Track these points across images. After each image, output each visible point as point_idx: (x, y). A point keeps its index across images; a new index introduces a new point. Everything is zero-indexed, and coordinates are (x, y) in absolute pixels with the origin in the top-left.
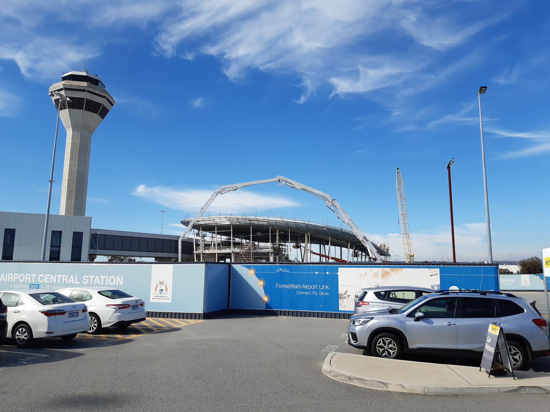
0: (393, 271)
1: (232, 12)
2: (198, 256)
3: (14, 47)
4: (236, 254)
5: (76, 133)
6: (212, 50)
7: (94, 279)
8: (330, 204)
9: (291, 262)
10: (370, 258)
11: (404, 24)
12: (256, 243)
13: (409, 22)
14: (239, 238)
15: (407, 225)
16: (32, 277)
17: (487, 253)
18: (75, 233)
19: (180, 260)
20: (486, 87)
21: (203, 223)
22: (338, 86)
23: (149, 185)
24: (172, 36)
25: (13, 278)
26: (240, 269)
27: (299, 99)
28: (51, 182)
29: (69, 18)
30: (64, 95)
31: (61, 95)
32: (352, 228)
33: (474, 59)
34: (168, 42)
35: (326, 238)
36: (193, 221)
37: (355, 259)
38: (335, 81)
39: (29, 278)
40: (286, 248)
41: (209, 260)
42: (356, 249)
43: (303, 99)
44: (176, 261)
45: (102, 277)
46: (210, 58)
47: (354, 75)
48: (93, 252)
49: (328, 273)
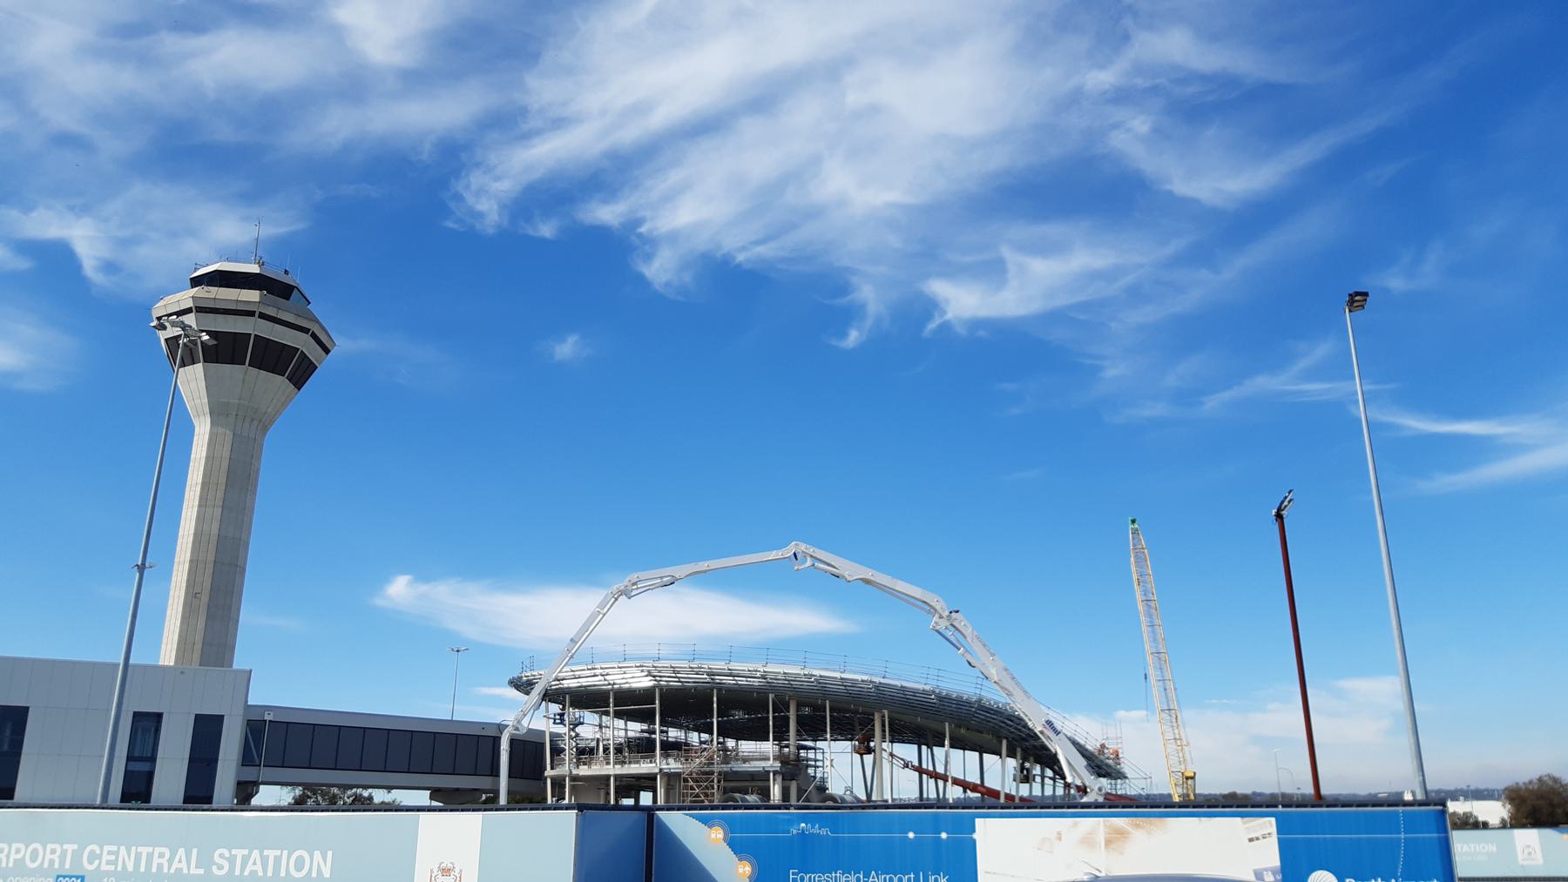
0: (1137, 826)
1: (659, 119)
2: (558, 784)
3: (71, 208)
4: (671, 778)
5: (221, 430)
6: (607, 213)
7: (245, 859)
8: (943, 624)
9: (837, 803)
10: (1067, 786)
11: (1118, 141)
12: (731, 743)
13: (1132, 137)
14: (679, 726)
15: (1170, 685)
16: (64, 853)
17: (1409, 765)
18: (199, 719)
19: (503, 800)
20: (1366, 294)
21: (573, 684)
22: (947, 301)
23: (423, 575)
24: (498, 179)
25: (8, 857)
26: (679, 823)
27: (843, 335)
28: (141, 568)
29: (224, 133)
30: (194, 326)
31: (184, 327)
32: (1009, 694)
33: (1313, 229)
34: (488, 194)
35: (933, 725)
36: (546, 678)
37: (1024, 790)
38: (940, 288)
39: (56, 857)
40: (819, 757)
41: (591, 800)
42: (1024, 759)
43: (853, 337)
44: (491, 804)
45: (271, 854)
46: (602, 235)
47: (992, 271)
48: (250, 774)
49: (944, 835)
